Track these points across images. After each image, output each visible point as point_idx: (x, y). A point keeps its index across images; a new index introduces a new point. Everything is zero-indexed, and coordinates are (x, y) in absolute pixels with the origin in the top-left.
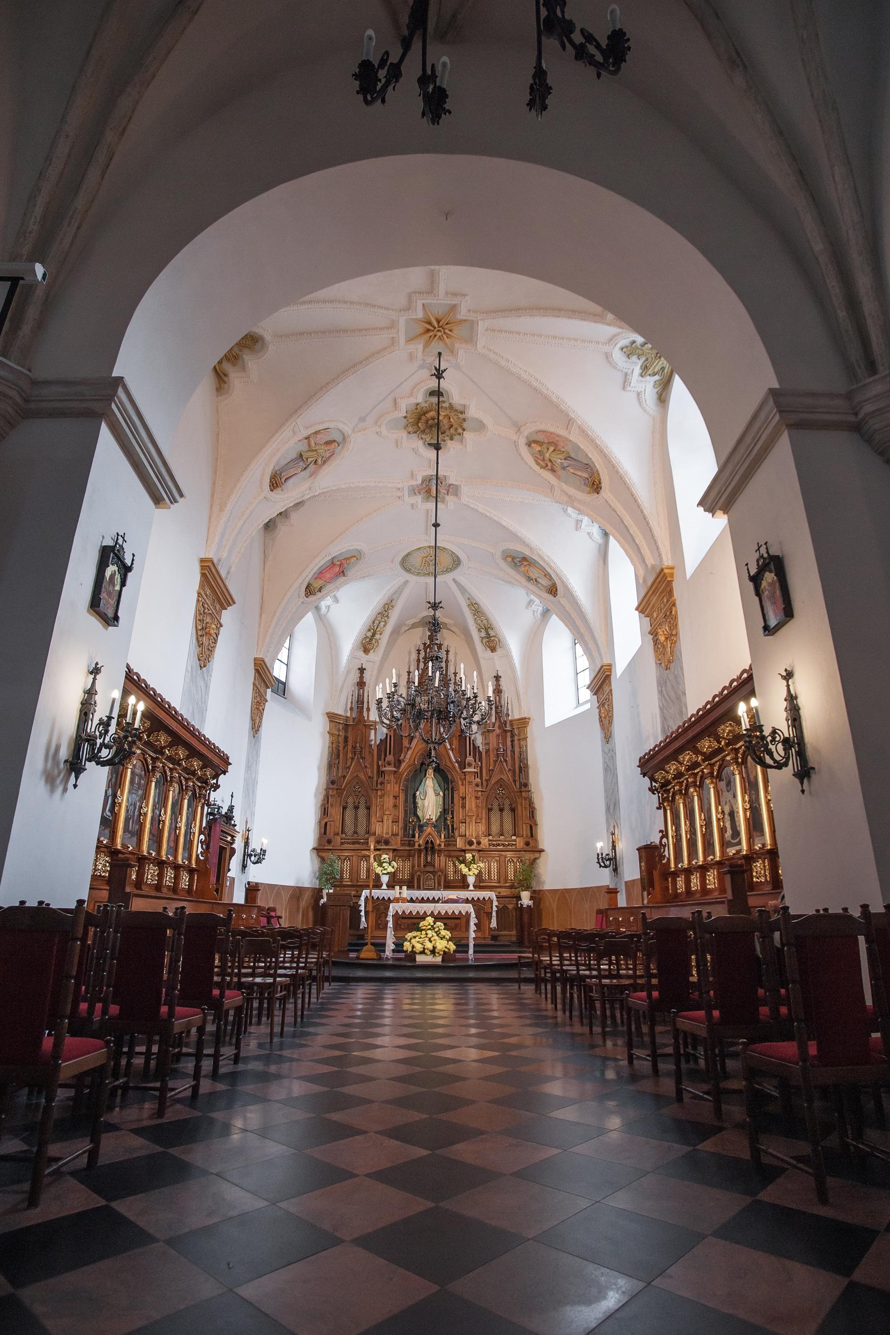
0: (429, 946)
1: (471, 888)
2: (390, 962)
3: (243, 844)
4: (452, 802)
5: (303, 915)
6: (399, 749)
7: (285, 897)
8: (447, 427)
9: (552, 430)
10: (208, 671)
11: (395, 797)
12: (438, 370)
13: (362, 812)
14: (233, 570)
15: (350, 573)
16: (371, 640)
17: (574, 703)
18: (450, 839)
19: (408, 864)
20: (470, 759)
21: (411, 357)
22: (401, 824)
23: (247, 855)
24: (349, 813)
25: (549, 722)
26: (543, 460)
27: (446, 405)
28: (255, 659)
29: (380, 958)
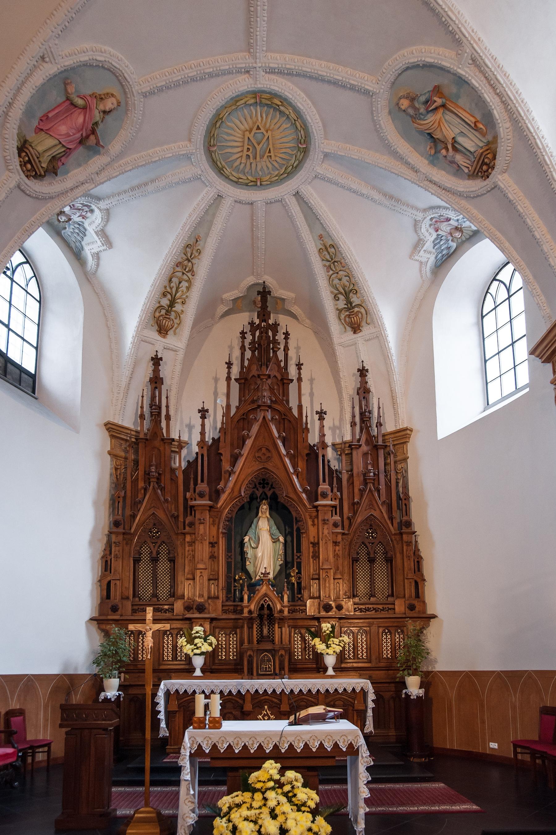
1: (330, 672)
4: (299, 550)
6: (216, 475)
7: (43, 693)
11: (213, 545)
13: (163, 566)
16: (168, 312)
17: (480, 403)
19: (233, 640)
20: (324, 487)
22: (222, 581)
24: (145, 569)
25: (442, 433)
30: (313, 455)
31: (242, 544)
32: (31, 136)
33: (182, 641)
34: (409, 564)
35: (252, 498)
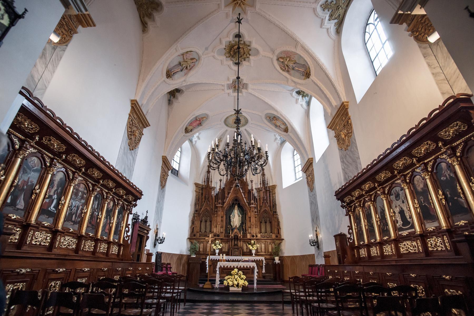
0: (236, 283)
1: (254, 255)
2: (218, 291)
3: (155, 235)
4: (245, 219)
5: (183, 266)
6: (224, 198)
7: (175, 259)
8: (242, 54)
9: (288, 49)
10: (135, 152)
11: (222, 217)
12: (239, 19)
13: (208, 223)
14: (149, 111)
15: (204, 125)
18: (245, 235)
19: (227, 245)
20: (252, 201)
21: (227, 15)
22: (224, 228)
23: (156, 240)
26: (284, 67)
27: (242, 42)
28: (163, 156)
29: (213, 288)
30: (250, 192)
31: (230, 217)
32: (188, 127)
33: (213, 245)
34: (276, 224)
35: (233, 204)
